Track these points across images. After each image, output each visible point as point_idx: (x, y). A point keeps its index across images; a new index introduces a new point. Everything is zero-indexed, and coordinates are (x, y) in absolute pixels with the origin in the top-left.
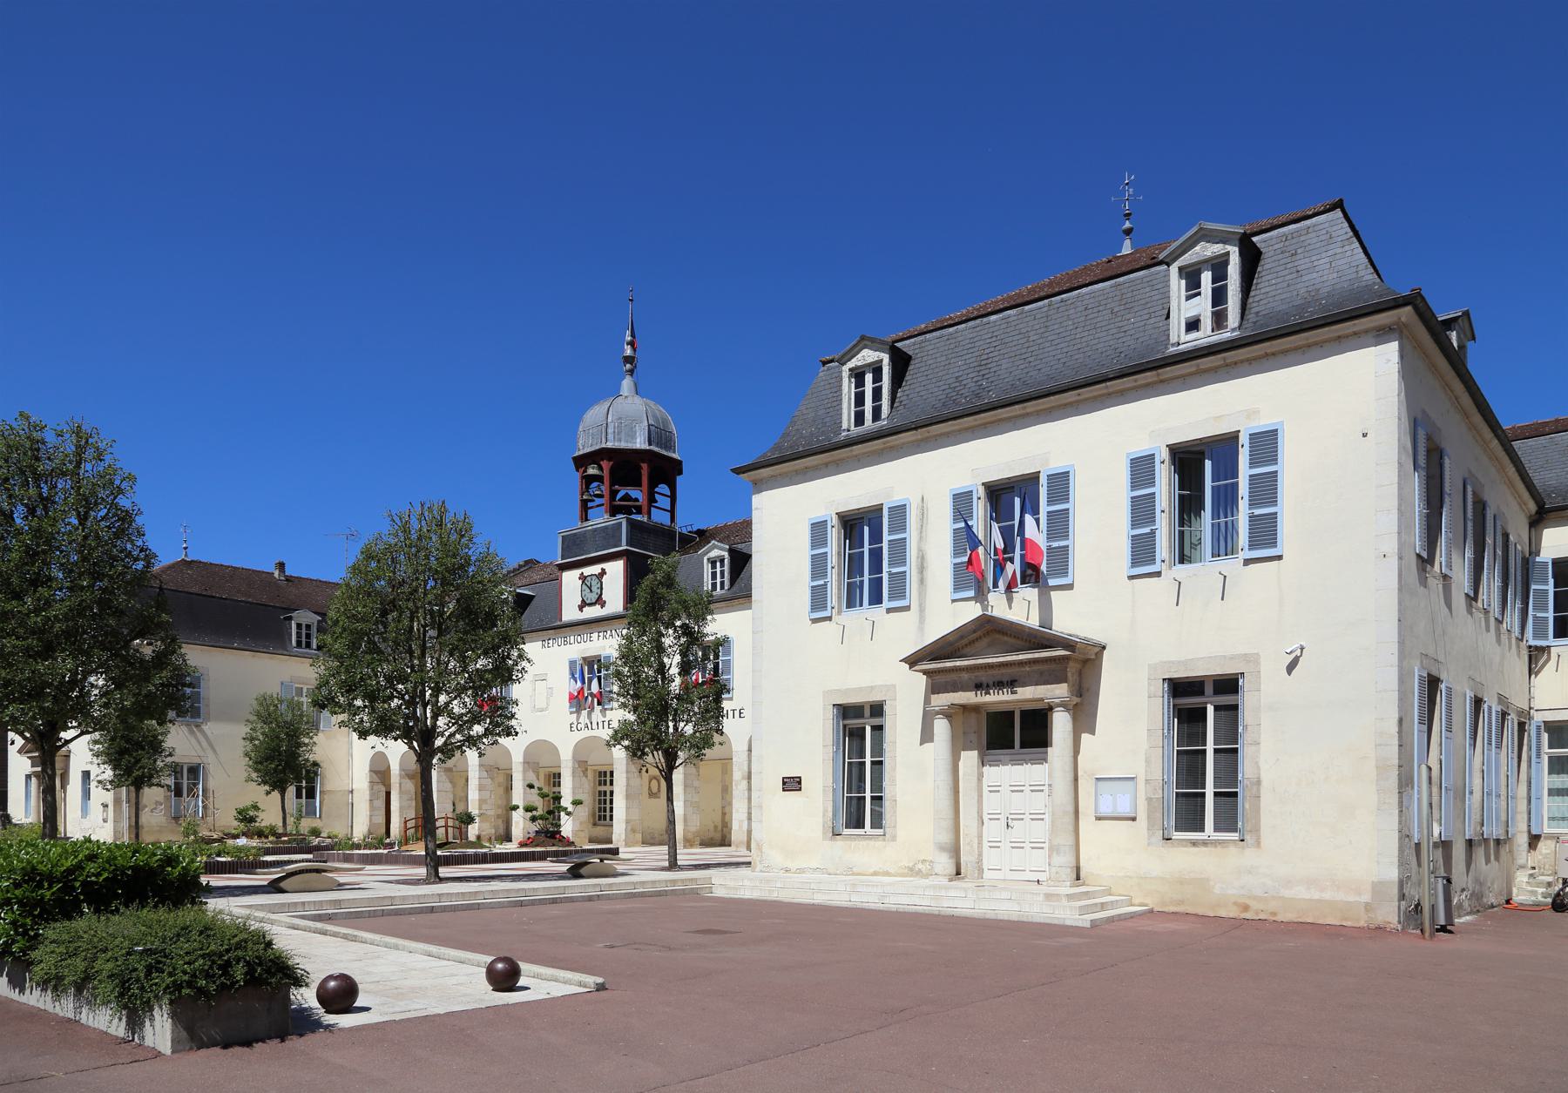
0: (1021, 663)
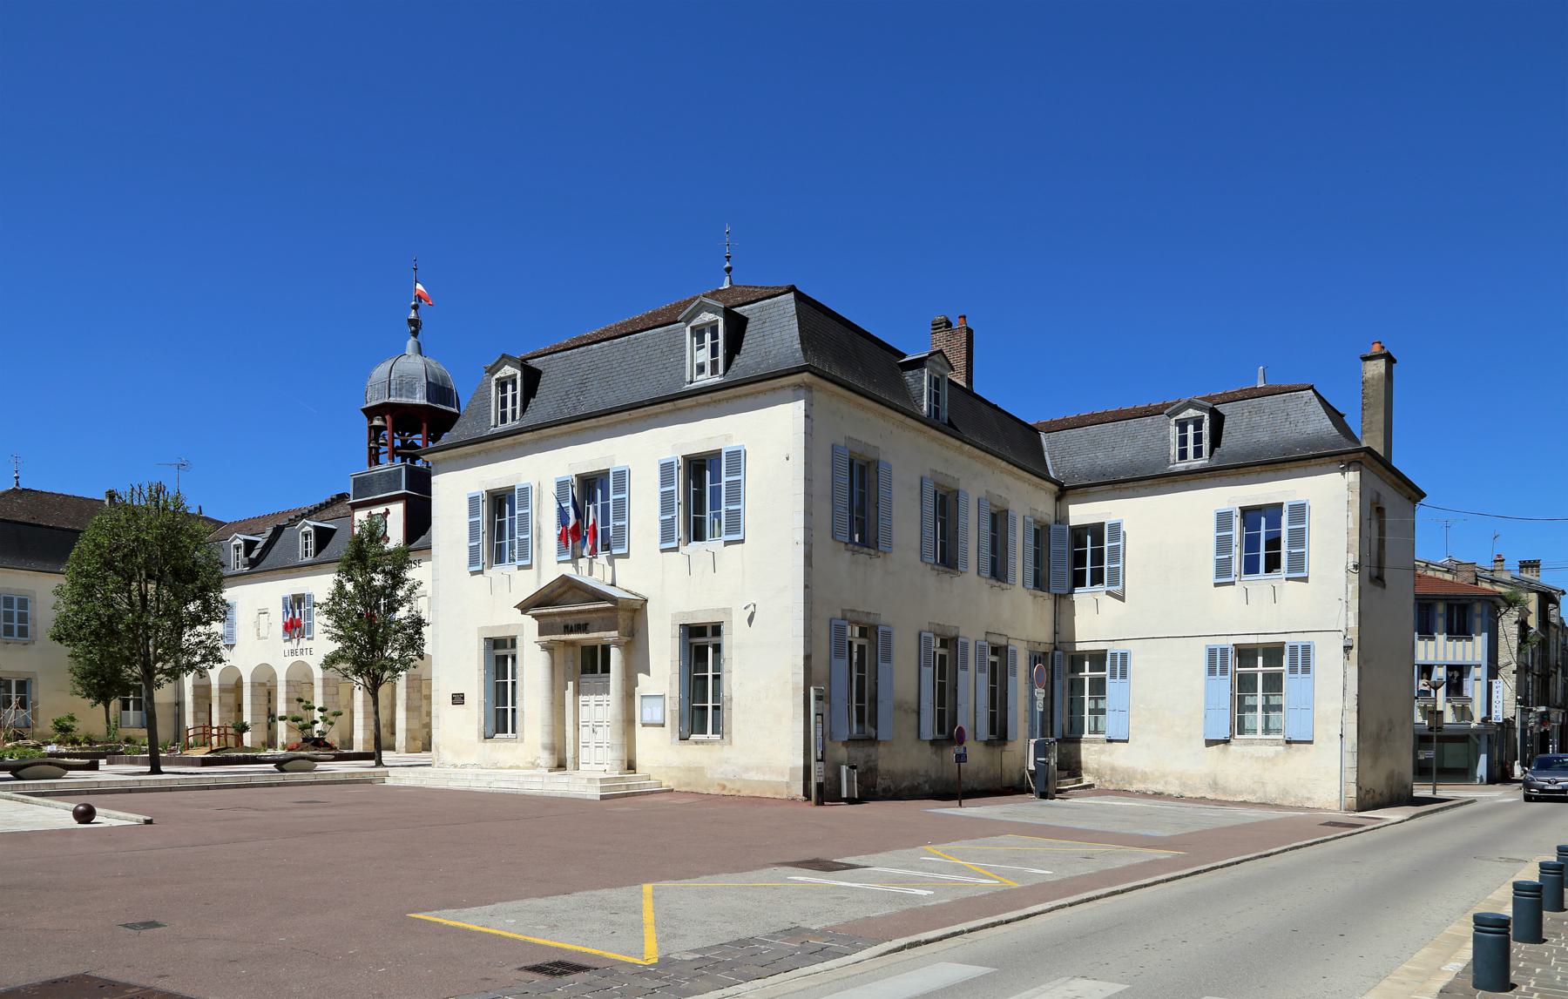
0: (589, 611)
